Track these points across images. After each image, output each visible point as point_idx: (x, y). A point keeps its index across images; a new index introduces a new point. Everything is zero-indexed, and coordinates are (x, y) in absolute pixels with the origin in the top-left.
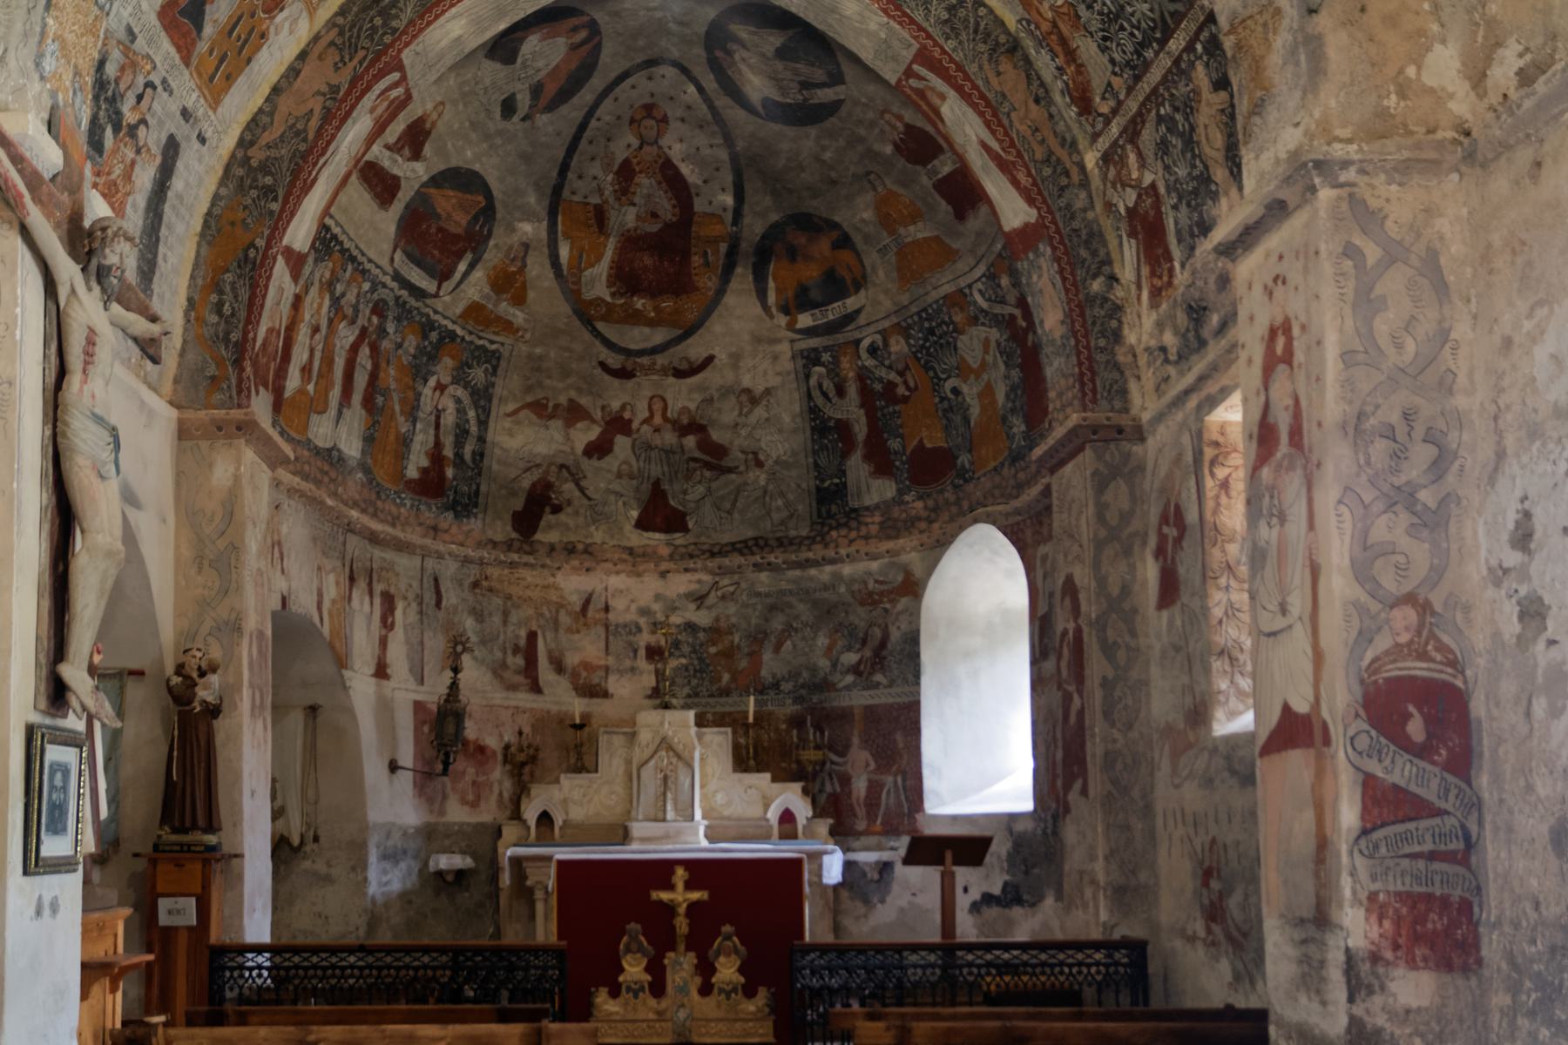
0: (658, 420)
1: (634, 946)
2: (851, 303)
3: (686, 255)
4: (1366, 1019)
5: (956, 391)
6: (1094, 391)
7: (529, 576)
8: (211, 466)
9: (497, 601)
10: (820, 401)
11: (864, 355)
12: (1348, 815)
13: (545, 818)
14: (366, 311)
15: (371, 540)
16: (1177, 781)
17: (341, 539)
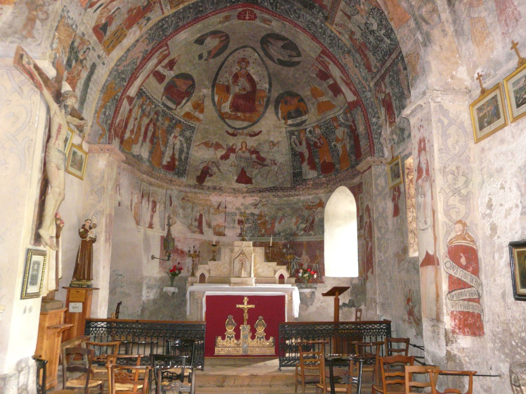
0: (244, 149)
1: (230, 323)
2: (304, 118)
3: (254, 101)
4: (451, 351)
5: (335, 146)
6: (374, 150)
7: (201, 196)
8: (98, 161)
9: (190, 204)
10: (294, 146)
11: (307, 133)
12: (445, 287)
13: (202, 276)
14: (152, 114)
15: (150, 184)
16: (400, 270)
17: (140, 184)
